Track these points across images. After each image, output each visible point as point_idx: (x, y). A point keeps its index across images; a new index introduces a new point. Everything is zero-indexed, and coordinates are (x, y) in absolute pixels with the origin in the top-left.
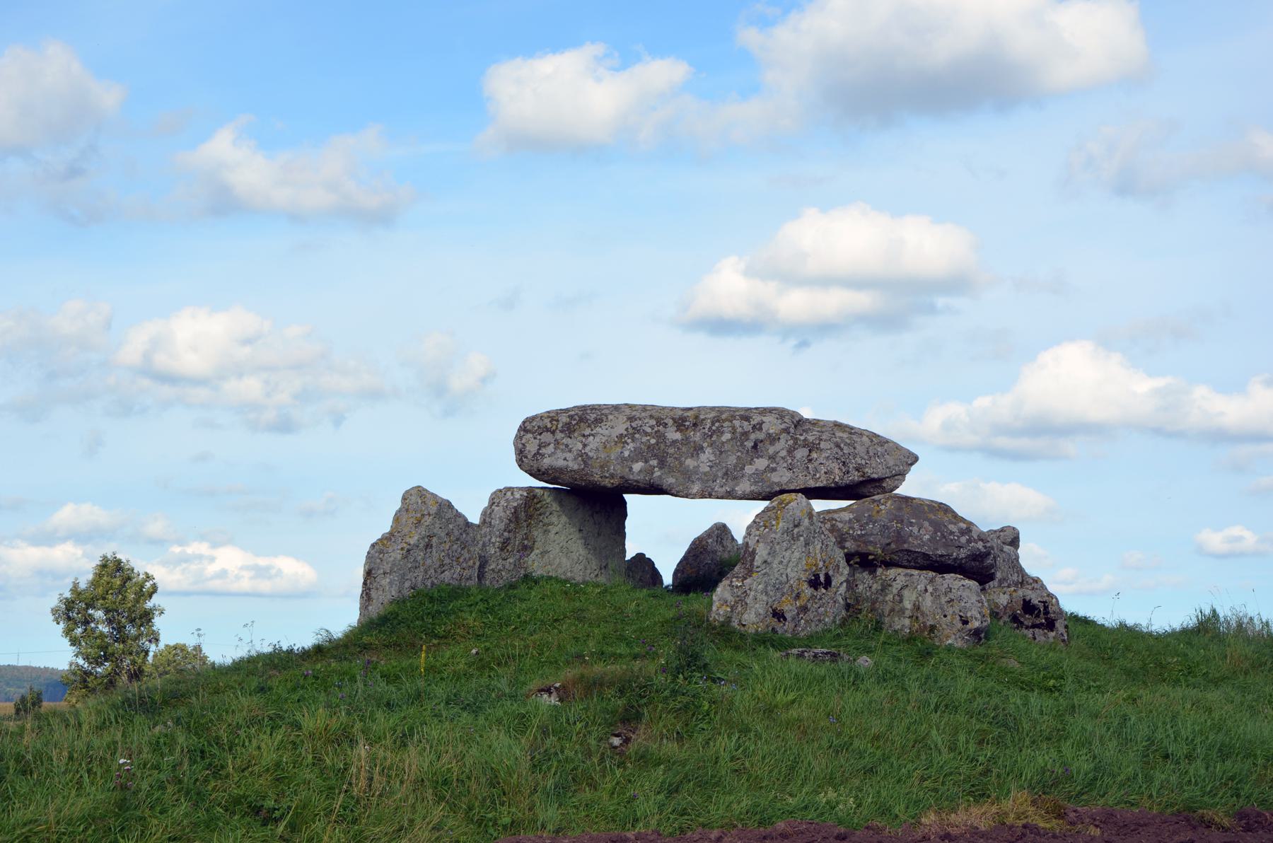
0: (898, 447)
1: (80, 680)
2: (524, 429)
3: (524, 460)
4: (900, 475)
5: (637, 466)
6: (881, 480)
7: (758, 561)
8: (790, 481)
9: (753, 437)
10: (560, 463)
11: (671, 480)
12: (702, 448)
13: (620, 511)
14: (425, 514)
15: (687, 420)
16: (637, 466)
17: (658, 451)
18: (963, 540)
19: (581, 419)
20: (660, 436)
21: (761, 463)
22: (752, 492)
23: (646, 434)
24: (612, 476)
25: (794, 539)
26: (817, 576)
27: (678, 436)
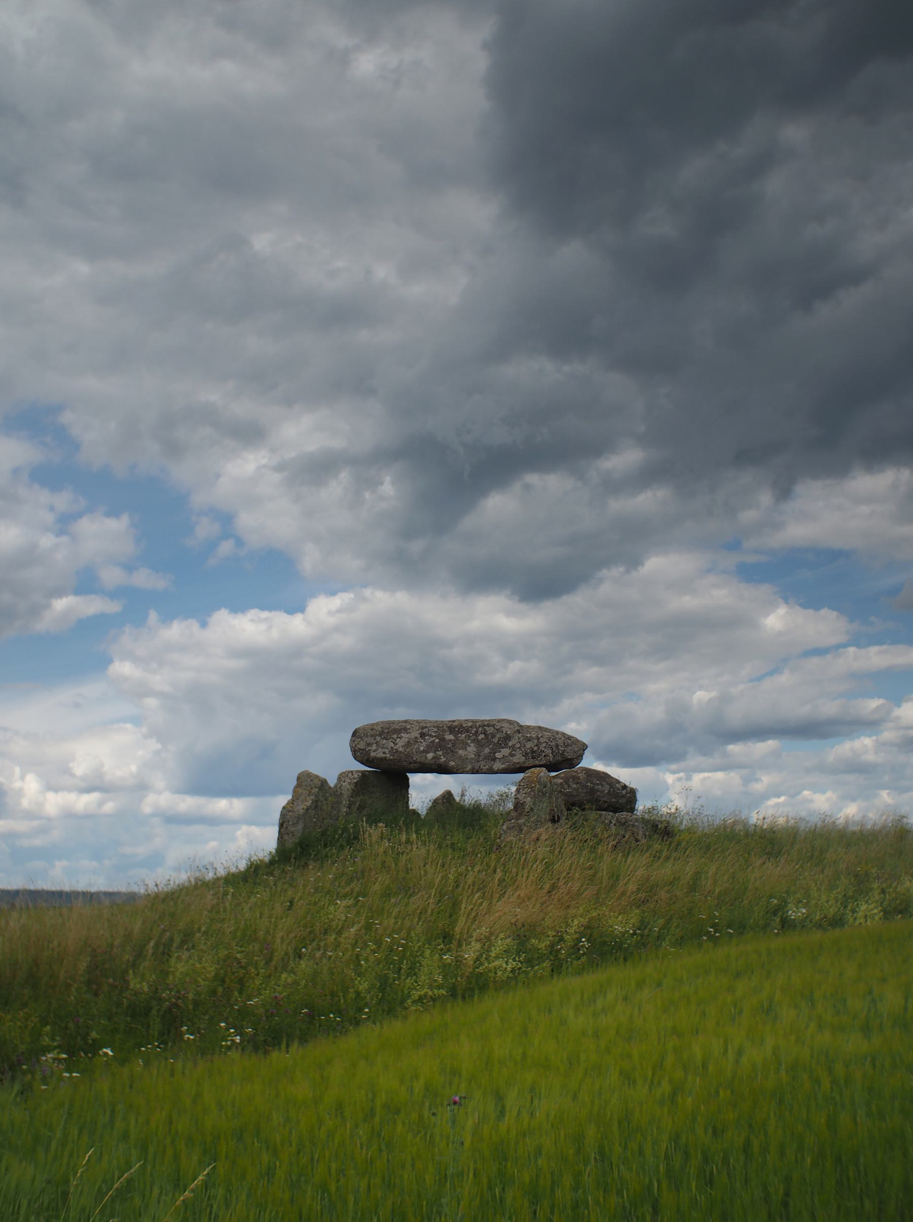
0: (577, 740)
1: (330, 788)
2: (355, 733)
3: (359, 754)
4: (580, 757)
5: (430, 756)
6: (572, 759)
7: (527, 808)
8: (524, 762)
9: (498, 736)
10: (381, 755)
11: (452, 763)
12: (467, 744)
13: (406, 784)
14: (307, 783)
15: (456, 728)
16: (430, 756)
17: (442, 744)
18: (624, 792)
19: (389, 730)
20: (442, 739)
21: (506, 751)
22: (503, 769)
23: (431, 736)
24: (415, 762)
25: (544, 794)
26: (554, 817)
27: (451, 737)
